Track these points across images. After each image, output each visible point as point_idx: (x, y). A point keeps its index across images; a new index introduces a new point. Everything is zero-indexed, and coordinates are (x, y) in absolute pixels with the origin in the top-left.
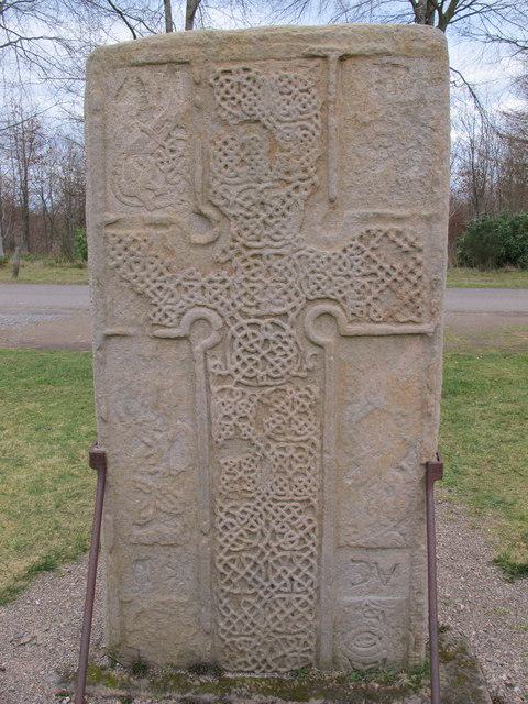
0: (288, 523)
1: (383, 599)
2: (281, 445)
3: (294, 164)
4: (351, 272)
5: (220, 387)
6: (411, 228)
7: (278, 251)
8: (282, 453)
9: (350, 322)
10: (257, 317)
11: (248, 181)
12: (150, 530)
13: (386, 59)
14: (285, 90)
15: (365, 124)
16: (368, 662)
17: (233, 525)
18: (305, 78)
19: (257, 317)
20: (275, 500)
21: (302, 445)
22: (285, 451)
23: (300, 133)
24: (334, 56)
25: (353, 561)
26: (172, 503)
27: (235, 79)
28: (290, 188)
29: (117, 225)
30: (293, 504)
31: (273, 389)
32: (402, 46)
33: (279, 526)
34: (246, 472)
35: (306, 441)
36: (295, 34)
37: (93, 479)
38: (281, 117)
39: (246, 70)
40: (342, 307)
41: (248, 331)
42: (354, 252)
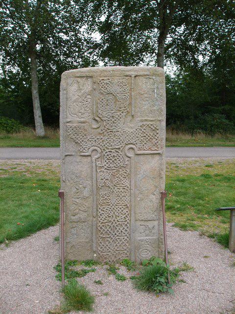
3: (122, 106)
15: (142, 95)
20: (116, 205)
24: (133, 76)
27: (105, 82)
41: (109, 153)
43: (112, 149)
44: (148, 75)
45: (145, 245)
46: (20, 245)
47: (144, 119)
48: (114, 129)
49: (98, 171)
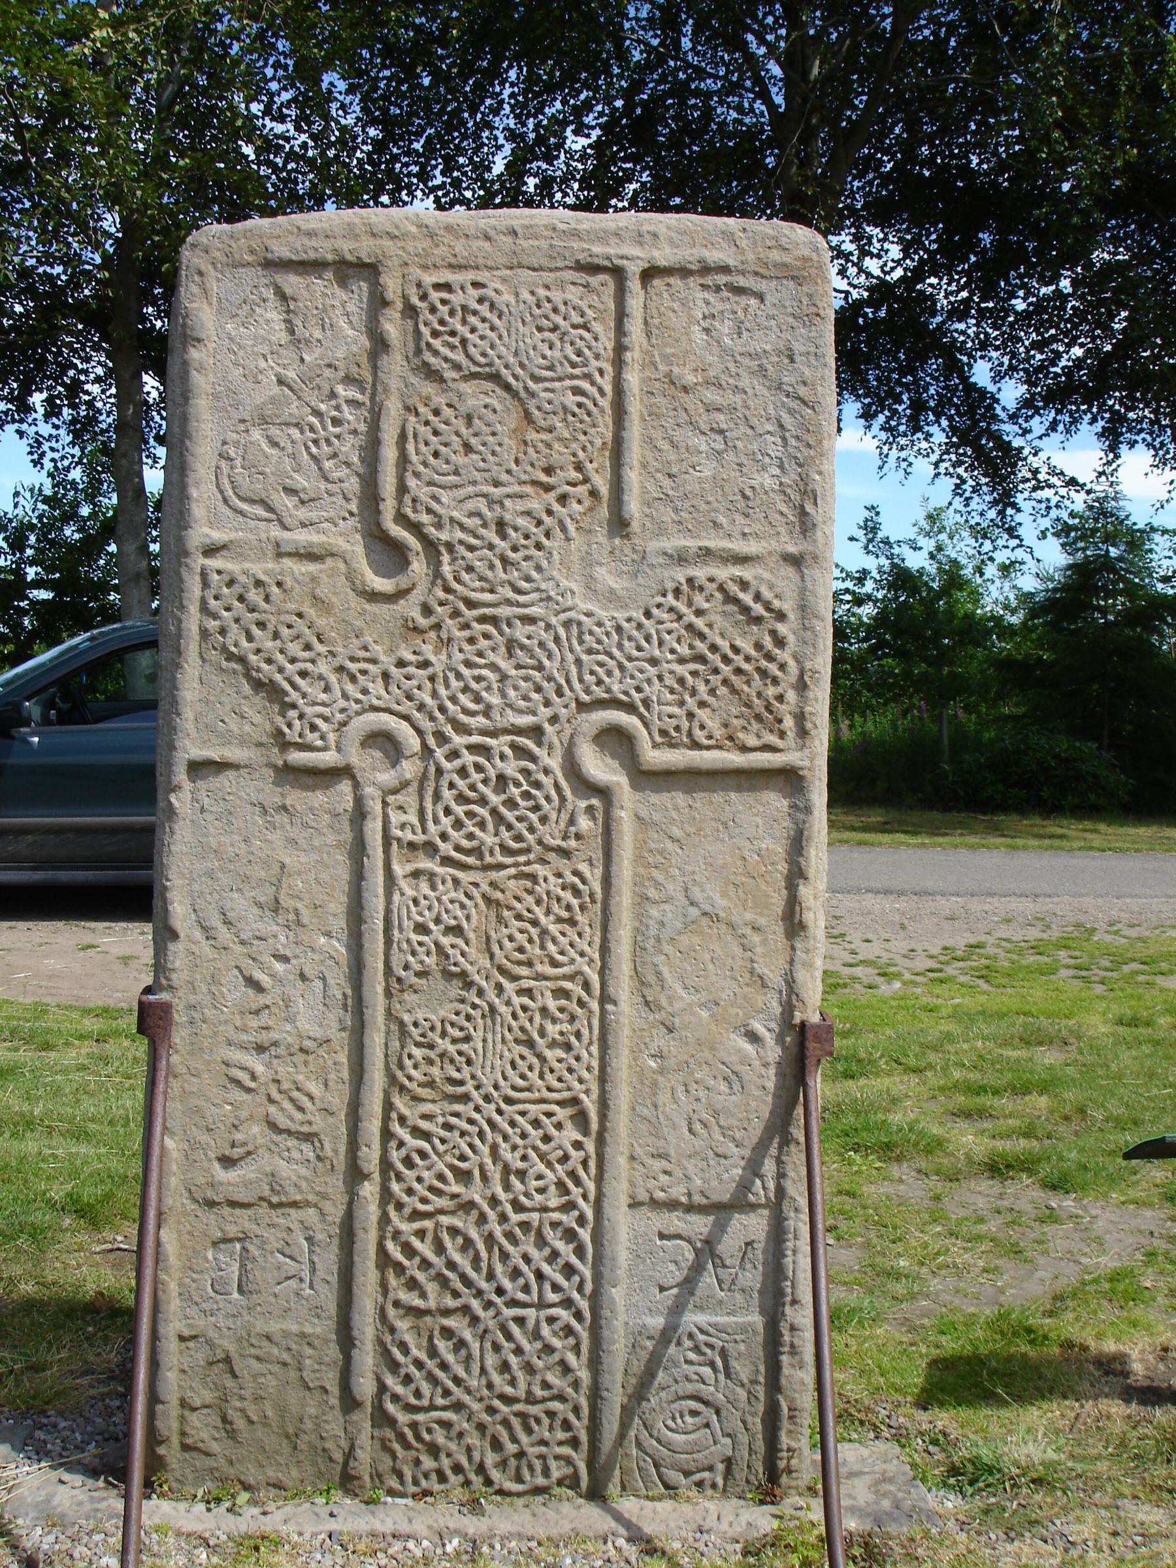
0: (535, 1148)
1: (720, 1320)
2: (526, 983)
3: (560, 454)
4: (657, 653)
5: (409, 868)
6: (767, 575)
7: (527, 611)
8: (526, 1000)
9: (655, 746)
10: (484, 732)
11: (474, 483)
12: (785, 510)
13: (722, 279)
14: (545, 323)
15: (685, 389)
16: (692, 1466)
17: (423, 1155)
18: (583, 305)
19: (484, 732)
20: (509, 1101)
21: (568, 985)
22: (532, 999)
23: (571, 400)
24: (634, 269)
25: (662, 1236)
26: (301, 1109)
27: (457, 299)
28: (551, 497)
29: (224, 553)
30: (545, 1107)
31: (513, 871)
32: (751, 257)
33: (518, 1154)
34: (454, 1041)
35: (571, 978)
36: (564, 227)
37: (141, 1048)
38: (537, 371)
39: (476, 285)
40: (641, 718)
41: (468, 758)
42: (665, 616)
43: (493, 734)
44: (725, 269)
45: (689, 1370)
46: (355, 319)
47: (692, 543)
48: (509, 602)
49: (398, 869)
